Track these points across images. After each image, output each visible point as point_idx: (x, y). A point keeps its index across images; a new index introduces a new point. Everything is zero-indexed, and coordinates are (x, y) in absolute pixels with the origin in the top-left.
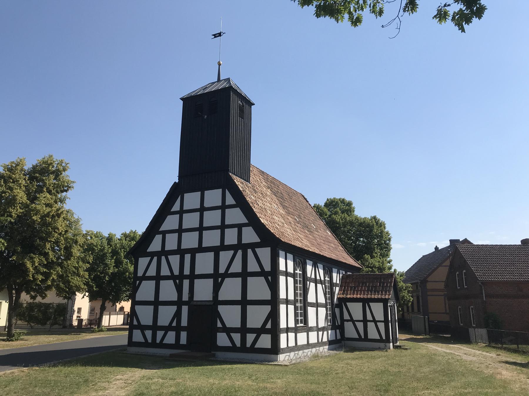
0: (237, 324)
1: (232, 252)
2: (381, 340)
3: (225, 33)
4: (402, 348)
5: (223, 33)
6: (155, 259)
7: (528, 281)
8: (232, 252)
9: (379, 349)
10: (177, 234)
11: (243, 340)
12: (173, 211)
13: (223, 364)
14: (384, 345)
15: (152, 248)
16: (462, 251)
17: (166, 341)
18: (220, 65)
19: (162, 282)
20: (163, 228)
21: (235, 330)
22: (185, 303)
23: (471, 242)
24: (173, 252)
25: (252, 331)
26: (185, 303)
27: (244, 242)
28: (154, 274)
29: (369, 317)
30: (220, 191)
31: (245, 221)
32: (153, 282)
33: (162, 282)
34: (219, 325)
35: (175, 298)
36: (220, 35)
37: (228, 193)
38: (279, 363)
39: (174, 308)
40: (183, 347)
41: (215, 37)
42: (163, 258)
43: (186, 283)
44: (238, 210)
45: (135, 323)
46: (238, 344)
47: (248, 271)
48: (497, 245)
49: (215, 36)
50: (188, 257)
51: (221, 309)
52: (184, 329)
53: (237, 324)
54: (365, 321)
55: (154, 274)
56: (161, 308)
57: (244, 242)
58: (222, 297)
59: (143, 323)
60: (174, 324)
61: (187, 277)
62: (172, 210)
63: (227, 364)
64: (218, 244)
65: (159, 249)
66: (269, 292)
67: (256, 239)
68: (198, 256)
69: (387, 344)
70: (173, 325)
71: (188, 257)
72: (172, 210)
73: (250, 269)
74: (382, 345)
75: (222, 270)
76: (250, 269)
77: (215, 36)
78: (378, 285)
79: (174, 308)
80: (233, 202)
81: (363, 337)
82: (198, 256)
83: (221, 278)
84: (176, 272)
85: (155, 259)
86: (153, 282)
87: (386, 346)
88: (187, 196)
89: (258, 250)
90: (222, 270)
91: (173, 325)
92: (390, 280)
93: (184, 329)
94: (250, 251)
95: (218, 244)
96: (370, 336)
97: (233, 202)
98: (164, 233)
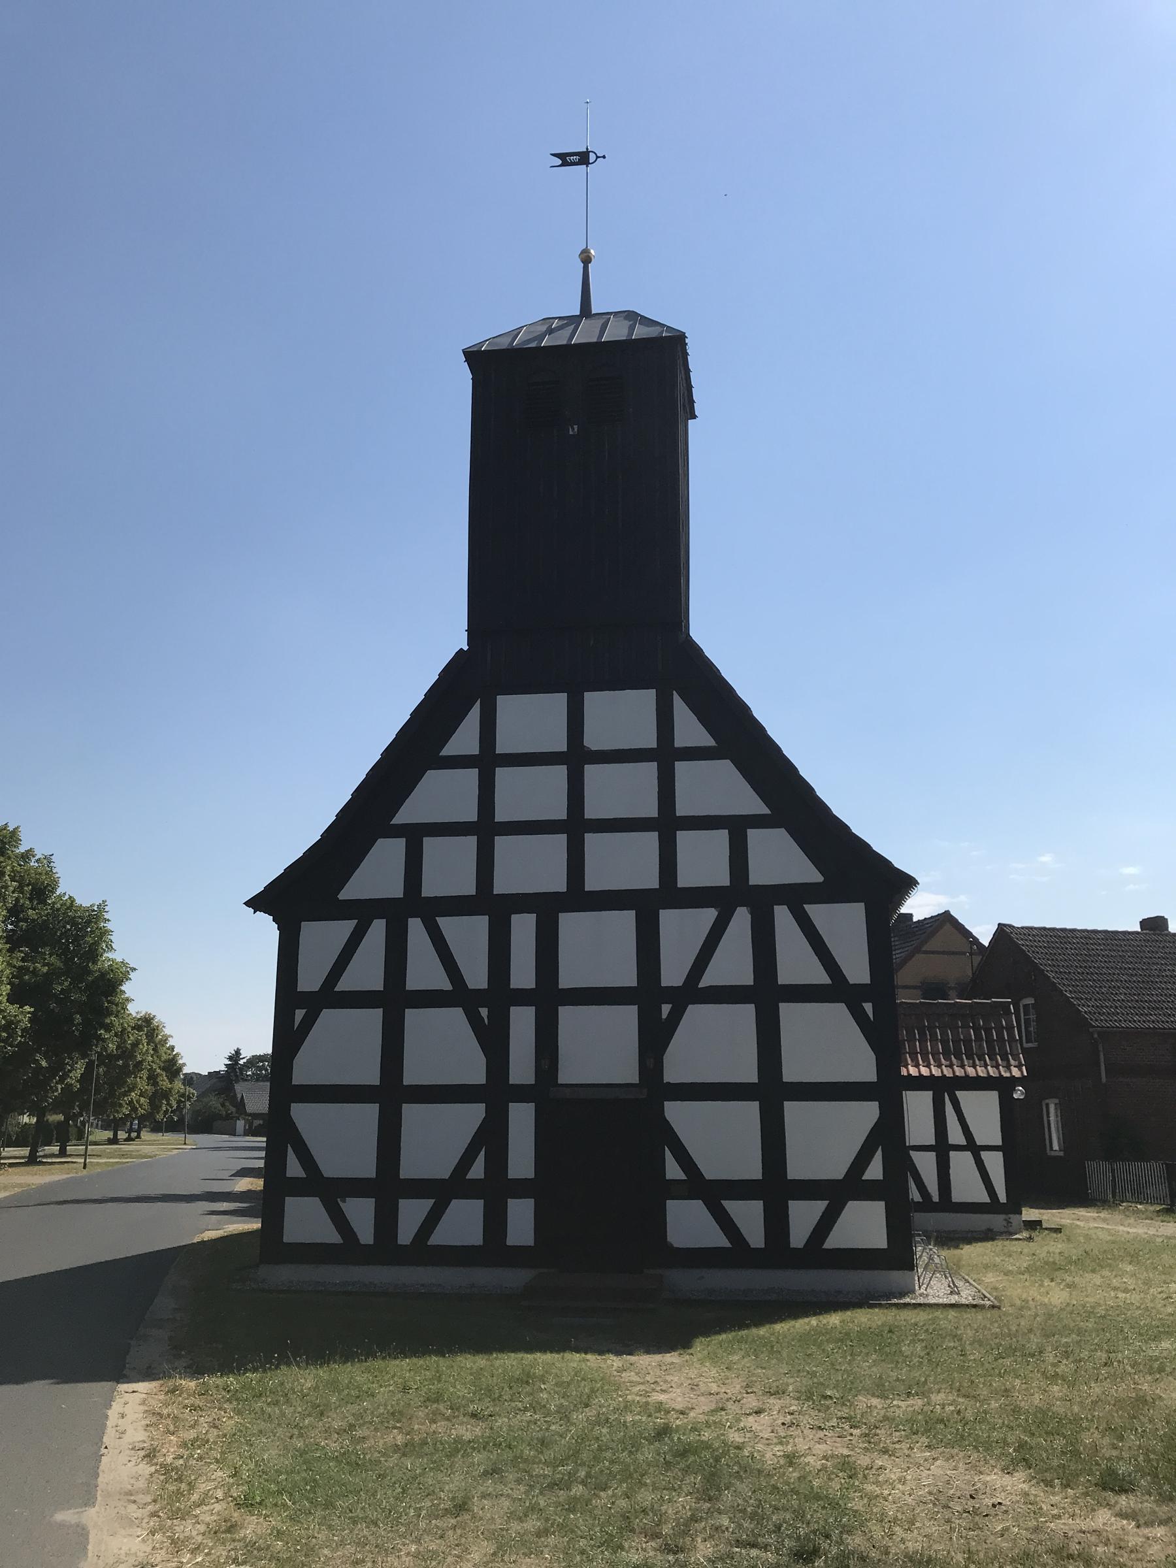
0: (365, 1166)
1: (709, 915)
2: (993, 1206)
3: (604, 157)
4: (1046, 1229)
5: (598, 157)
6: (378, 929)
7: (1175, 1029)
8: (709, 915)
9: (988, 1236)
10: (473, 840)
11: (386, 1221)
12: (444, 754)
13: (781, 1319)
14: (1005, 1220)
15: (357, 888)
16: (1023, 945)
17: (440, 1237)
18: (586, 259)
19: (413, 1017)
20: (409, 813)
21: (355, 1187)
22: (522, 1093)
23: (959, 921)
24: (458, 906)
25: (419, 1188)
26: (522, 1093)
27: (428, 891)
28: (376, 982)
29: (955, 1135)
30: (648, 697)
31: (755, 805)
32: (374, 1017)
33: (413, 1017)
34: (673, 1171)
35: (475, 1071)
36: (583, 158)
37: (680, 707)
38: (921, 1300)
39: (474, 1114)
40: (517, 1257)
41: (565, 164)
42: (415, 927)
43: (522, 1021)
44: (725, 772)
45: (294, 1168)
46: (366, 1234)
47: (635, 984)
48: (1095, 932)
49: (565, 159)
50: (524, 927)
51: (677, 1113)
52: (521, 1188)
53: (365, 1166)
54: (942, 1148)
55: (376, 982)
56: (412, 1113)
57: (428, 891)
58: (675, 1070)
59: (330, 1168)
60: (477, 1171)
61: (522, 997)
62: (444, 752)
63: (796, 1316)
64: (558, 883)
65: (394, 888)
66: (481, 1060)
67: (807, 873)
68: (570, 924)
69: (1011, 1216)
70: (867, 1176)
71: (524, 927)
72: (444, 752)
73: (414, 982)
74: (997, 1221)
75: (673, 974)
76: (414, 982)
77: (565, 159)
78: (971, 1036)
79: (474, 1114)
80: (705, 739)
81: (936, 1198)
82: (570, 924)
83: (670, 1006)
84: (477, 977)
85: (378, 929)
86: (374, 1017)
87: (1009, 1222)
88: (509, 707)
89: (814, 911)
90: (673, 974)
91: (867, 1176)
92: (960, 1023)
93: (521, 1188)
94: (782, 916)
95: (558, 883)
96: (957, 1196)
97: (705, 739)
98: (415, 835)
